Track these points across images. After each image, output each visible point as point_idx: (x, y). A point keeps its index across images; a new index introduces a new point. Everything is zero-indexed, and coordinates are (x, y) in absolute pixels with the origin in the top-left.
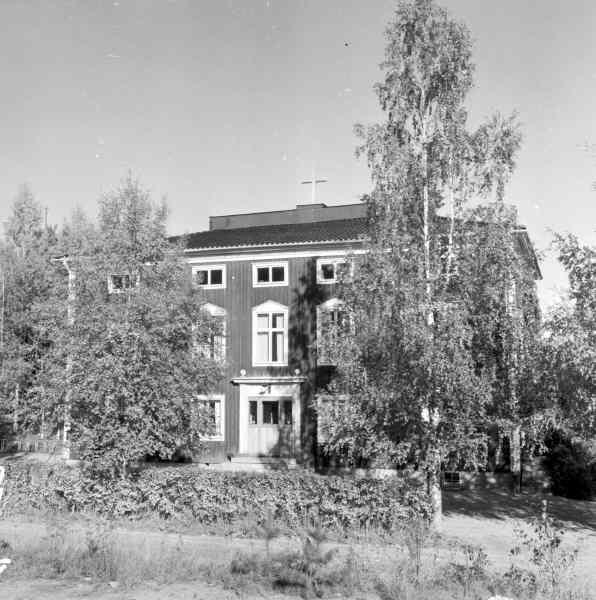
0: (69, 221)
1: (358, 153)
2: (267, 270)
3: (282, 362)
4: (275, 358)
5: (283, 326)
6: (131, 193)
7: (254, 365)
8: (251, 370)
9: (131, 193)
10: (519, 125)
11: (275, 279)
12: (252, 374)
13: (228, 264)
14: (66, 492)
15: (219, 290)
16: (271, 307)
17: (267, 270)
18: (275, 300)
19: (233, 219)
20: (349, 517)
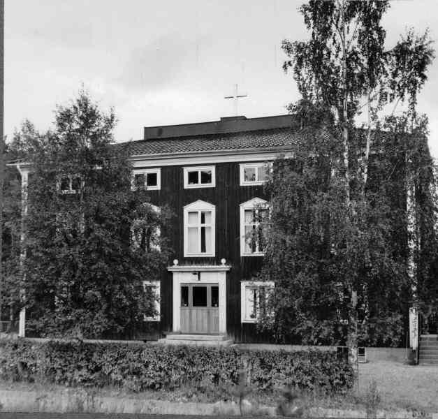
0: (19, 130)
1: (285, 67)
2: (197, 173)
3: (211, 252)
4: (203, 249)
5: (211, 222)
6: (83, 103)
7: (185, 256)
8: (184, 261)
9: (83, 103)
10: (430, 42)
11: (203, 182)
12: (184, 264)
13: (163, 168)
14: (29, 364)
15: (207, 189)
16: (200, 206)
17: (197, 173)
18: (204, 199)
19: (164, 129)
20: (23, 361)
